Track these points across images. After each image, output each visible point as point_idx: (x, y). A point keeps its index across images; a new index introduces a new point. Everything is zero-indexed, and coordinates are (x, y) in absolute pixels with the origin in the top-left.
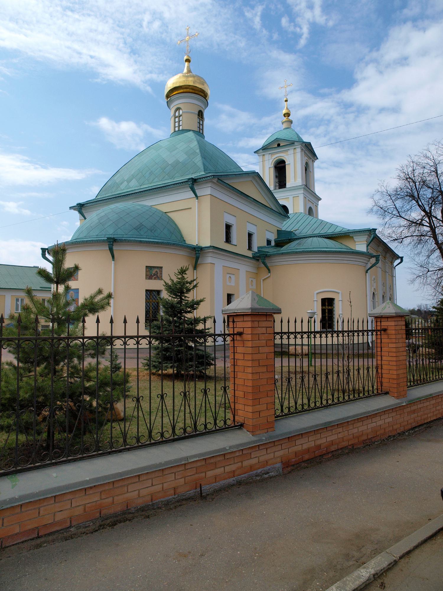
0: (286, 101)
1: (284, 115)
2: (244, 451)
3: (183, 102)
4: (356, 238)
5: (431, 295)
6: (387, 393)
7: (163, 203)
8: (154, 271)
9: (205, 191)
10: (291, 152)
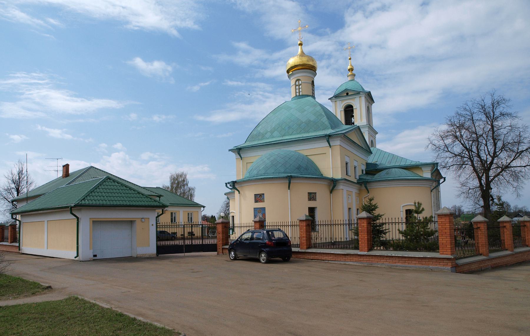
0: (350, 59)
1: (349, 70)
2: (483, 261)
3: (302, 75)
4: (423, 169)
6: (507, 250)
7: (304, 150)
9: (337, 143)
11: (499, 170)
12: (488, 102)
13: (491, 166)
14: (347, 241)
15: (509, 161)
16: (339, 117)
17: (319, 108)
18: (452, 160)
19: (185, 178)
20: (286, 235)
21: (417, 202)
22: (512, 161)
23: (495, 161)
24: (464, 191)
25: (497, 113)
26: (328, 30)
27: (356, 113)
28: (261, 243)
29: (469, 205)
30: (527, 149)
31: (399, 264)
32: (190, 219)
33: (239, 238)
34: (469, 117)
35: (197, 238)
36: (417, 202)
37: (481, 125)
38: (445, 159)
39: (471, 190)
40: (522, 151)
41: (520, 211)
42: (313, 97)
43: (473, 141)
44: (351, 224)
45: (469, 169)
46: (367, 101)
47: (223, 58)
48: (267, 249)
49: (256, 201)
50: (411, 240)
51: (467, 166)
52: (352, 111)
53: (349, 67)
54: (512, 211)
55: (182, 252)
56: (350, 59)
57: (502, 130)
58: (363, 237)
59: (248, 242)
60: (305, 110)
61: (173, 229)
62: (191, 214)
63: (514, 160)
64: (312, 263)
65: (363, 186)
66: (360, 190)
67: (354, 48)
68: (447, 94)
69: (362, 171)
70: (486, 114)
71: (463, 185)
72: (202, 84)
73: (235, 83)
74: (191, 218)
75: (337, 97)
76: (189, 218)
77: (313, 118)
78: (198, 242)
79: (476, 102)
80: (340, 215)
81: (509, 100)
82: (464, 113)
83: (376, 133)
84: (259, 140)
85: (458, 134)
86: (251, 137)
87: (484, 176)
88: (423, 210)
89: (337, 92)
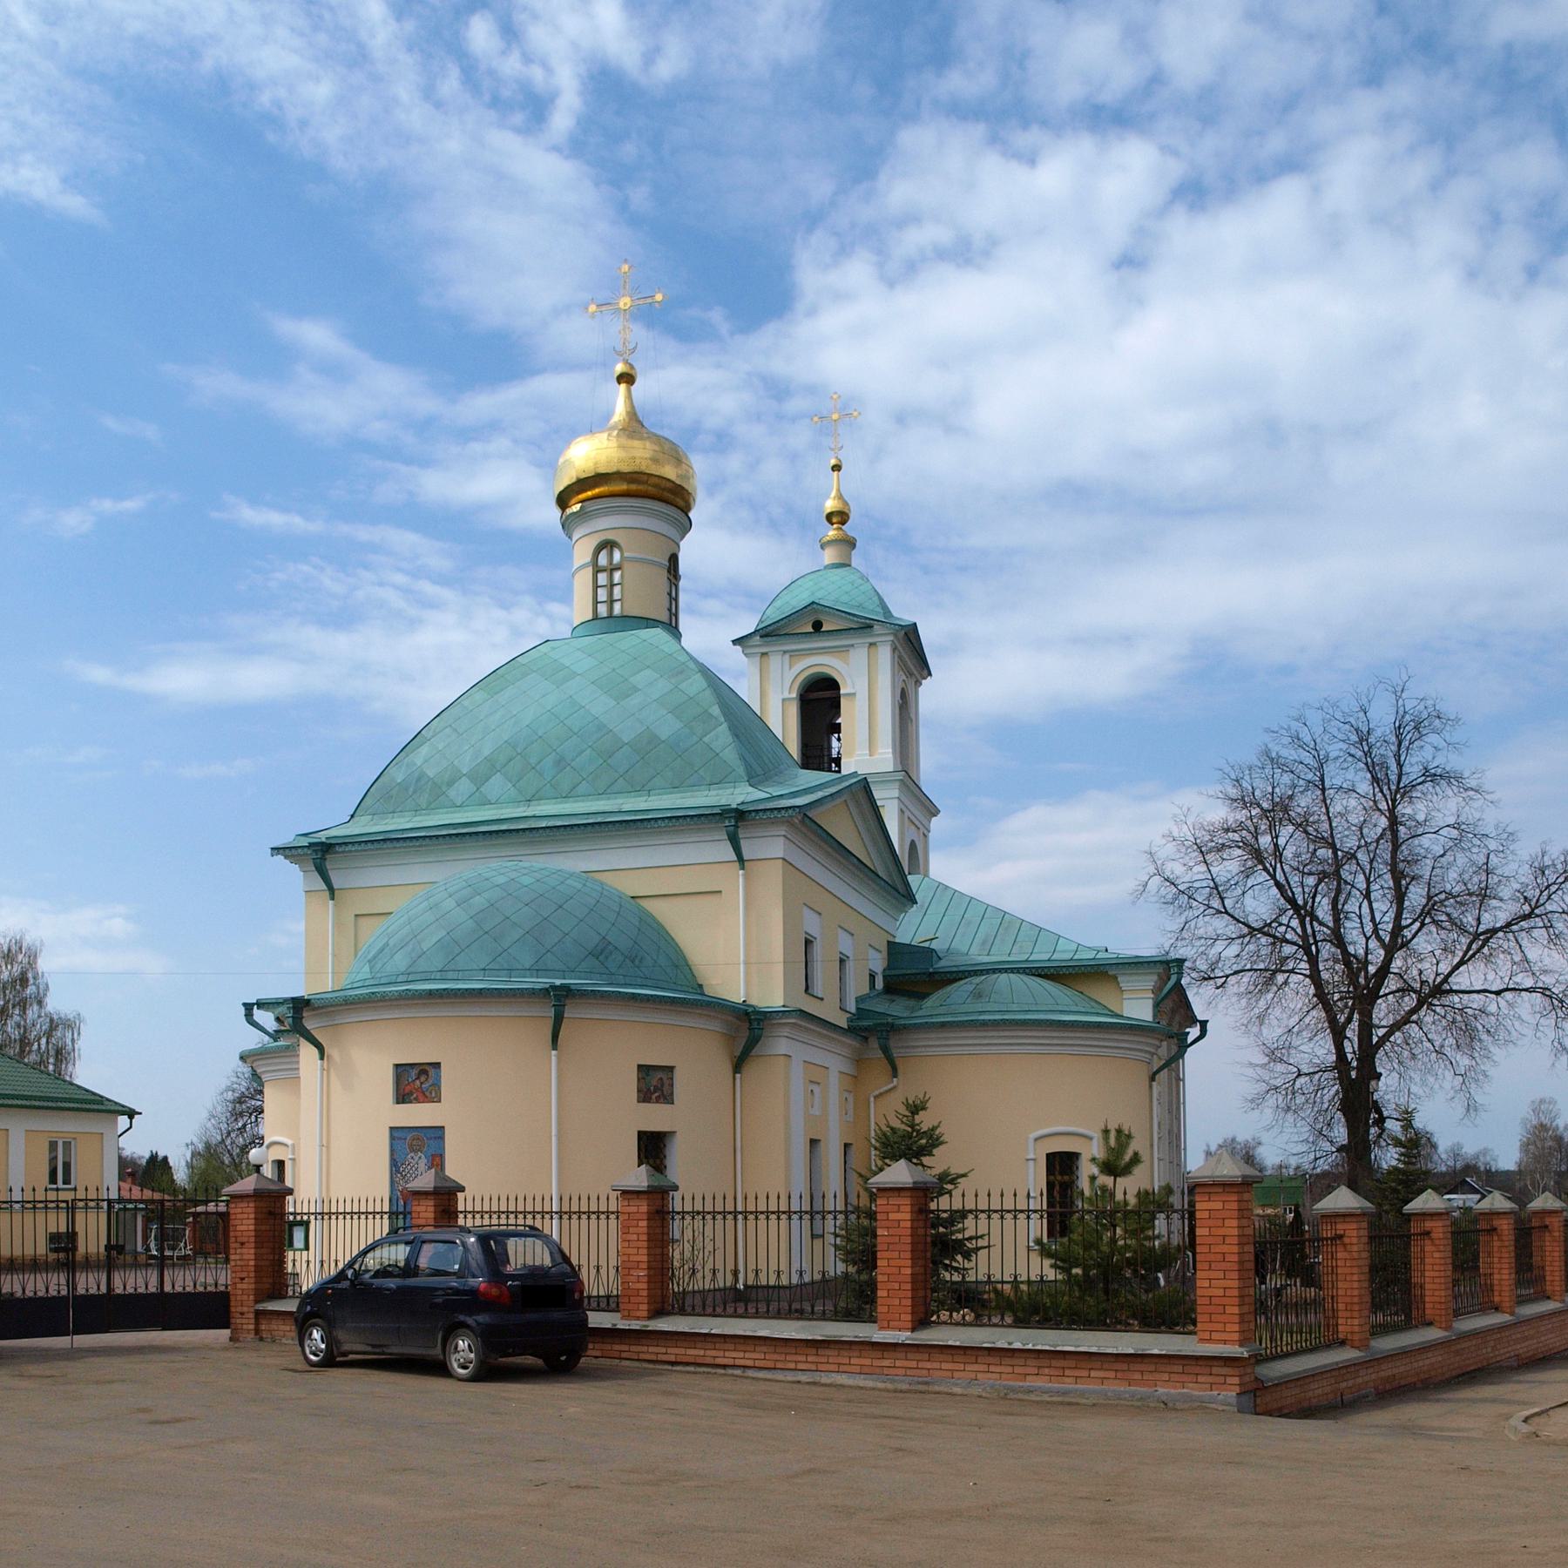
0: (837, 468)
1: (829, 517)
5: (1306, 1141)
6: (1430, 1324)
7: (628, 870)
8: (654, 1080)
9: (769, 847)
10: (859, 656)
11: (1410, 1001)
12: (1382, 719)
13: (1379, 985)
14: (802, 1286)
15: (1444, 968)
16: (775, 722)
17: (697, 684)
18: (1234, 949)
19: (32, 963)
20: (566, 1259)
21: (1112, 1127)
22: (1457, 967)
23: (1397, 964)
24: (1278, 1082)
25: (1413, 770)
26: (717, 316)
27: (852, 716)
28: (457, 1291)
29: (1289, 1143)
30: (1509, 925)
31: (1039, 1383)
32: (59, 1171)
33: (350, 1265)
34: (1310, 776)
35: (88, 1264)
36: (1112, 1127)
37: (1353, 809)
38: (1210, 942)
39: (1302, 1080)
40: (1494, 931)
41: (1470, 1169)
42: (672, 627)
43: (1322, 876)
44: (824, 1214)
45: (1298, 990)
46: (900, 664)
47: (218, 384)
48: (483, 1318)
49: (402, 1097)
50: (1086, 1284)
51: (1294, 978)
52: (835, 705)
53: (830, 505)
54: (1444, 1169)
55: (57, 1329)
56: (837, 468)
57: (1425, 841)
58: (895, 1269)
59: (391, 1283)
60: (636, 689)
61: (52, 1216)
62: (67, 1145)
63: (1462, 963)
64: (676, 1380)
65: (874, 1043)
66: (859, 1061)
67: (835, 416)
68: (1212, 663)
69: (872, 977)
70: (1370, 768)
71: (1275, 1055)
72: (107, 505)
73: (275, 519)
74: (67, 1166)
75: (770, 634)
76: (53, 1160)
77: (667, 727)
78: (89, 1283)
79: (1338, 715)
80: (777, 1174)
81: (1457, 720)
82: (1290, 754)
83: (934, 812)
84: (417, 811)
85: (1265, 841)
86: (378, 794)
87: (1355, 1025)
88: (1136, 1159)
89: (774, 615)
